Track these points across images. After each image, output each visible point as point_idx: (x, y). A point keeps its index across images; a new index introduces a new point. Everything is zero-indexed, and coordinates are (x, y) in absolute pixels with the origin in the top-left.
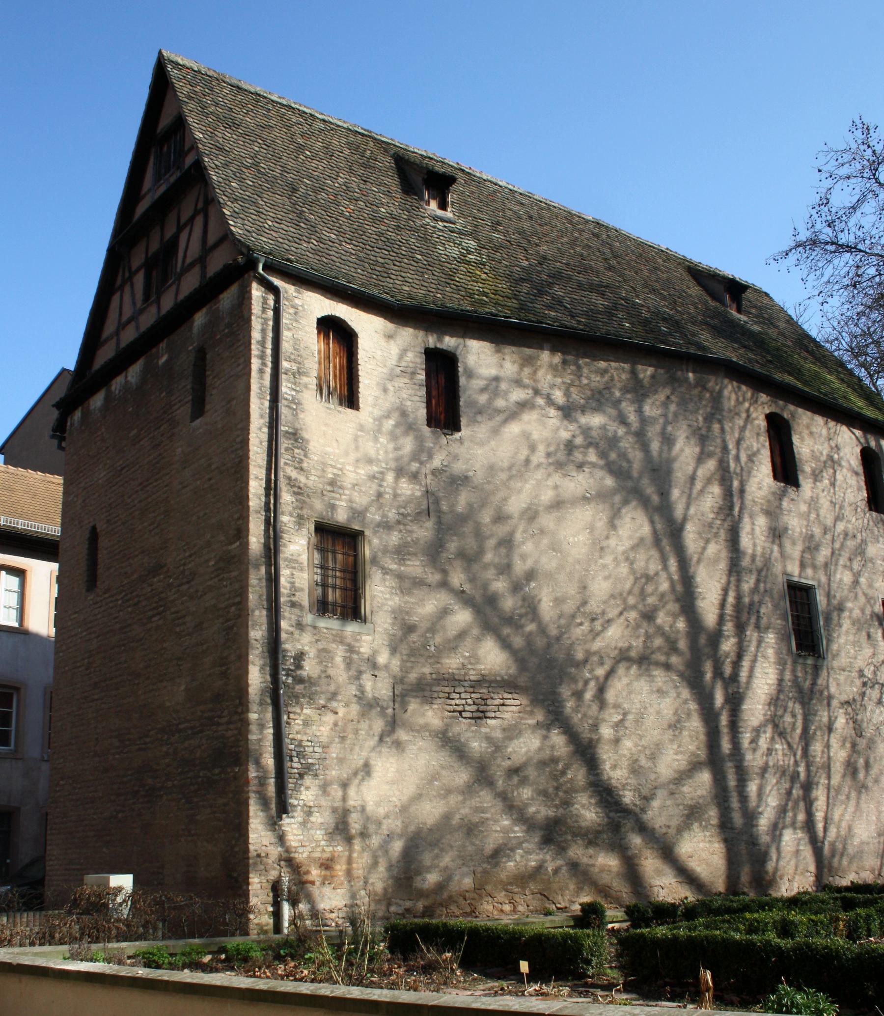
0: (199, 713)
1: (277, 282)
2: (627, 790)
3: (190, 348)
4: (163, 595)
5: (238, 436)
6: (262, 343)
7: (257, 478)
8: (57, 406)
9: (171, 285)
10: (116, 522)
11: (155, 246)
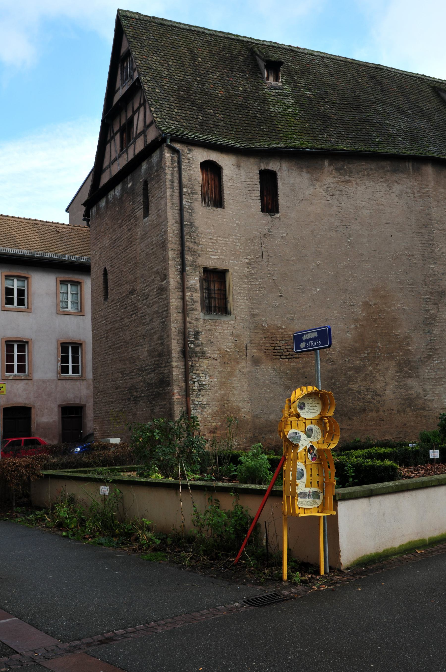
0: (153, 362)
1: (178, 146)
2: (369, 392)
3: (141, 180)
4: (136, 305)
5: (163, 228)
6: (172, 181)
7: (172, 249)
8: (84, 204)
9: (131, 144)
10: (115, 267)
11: (123, 121)
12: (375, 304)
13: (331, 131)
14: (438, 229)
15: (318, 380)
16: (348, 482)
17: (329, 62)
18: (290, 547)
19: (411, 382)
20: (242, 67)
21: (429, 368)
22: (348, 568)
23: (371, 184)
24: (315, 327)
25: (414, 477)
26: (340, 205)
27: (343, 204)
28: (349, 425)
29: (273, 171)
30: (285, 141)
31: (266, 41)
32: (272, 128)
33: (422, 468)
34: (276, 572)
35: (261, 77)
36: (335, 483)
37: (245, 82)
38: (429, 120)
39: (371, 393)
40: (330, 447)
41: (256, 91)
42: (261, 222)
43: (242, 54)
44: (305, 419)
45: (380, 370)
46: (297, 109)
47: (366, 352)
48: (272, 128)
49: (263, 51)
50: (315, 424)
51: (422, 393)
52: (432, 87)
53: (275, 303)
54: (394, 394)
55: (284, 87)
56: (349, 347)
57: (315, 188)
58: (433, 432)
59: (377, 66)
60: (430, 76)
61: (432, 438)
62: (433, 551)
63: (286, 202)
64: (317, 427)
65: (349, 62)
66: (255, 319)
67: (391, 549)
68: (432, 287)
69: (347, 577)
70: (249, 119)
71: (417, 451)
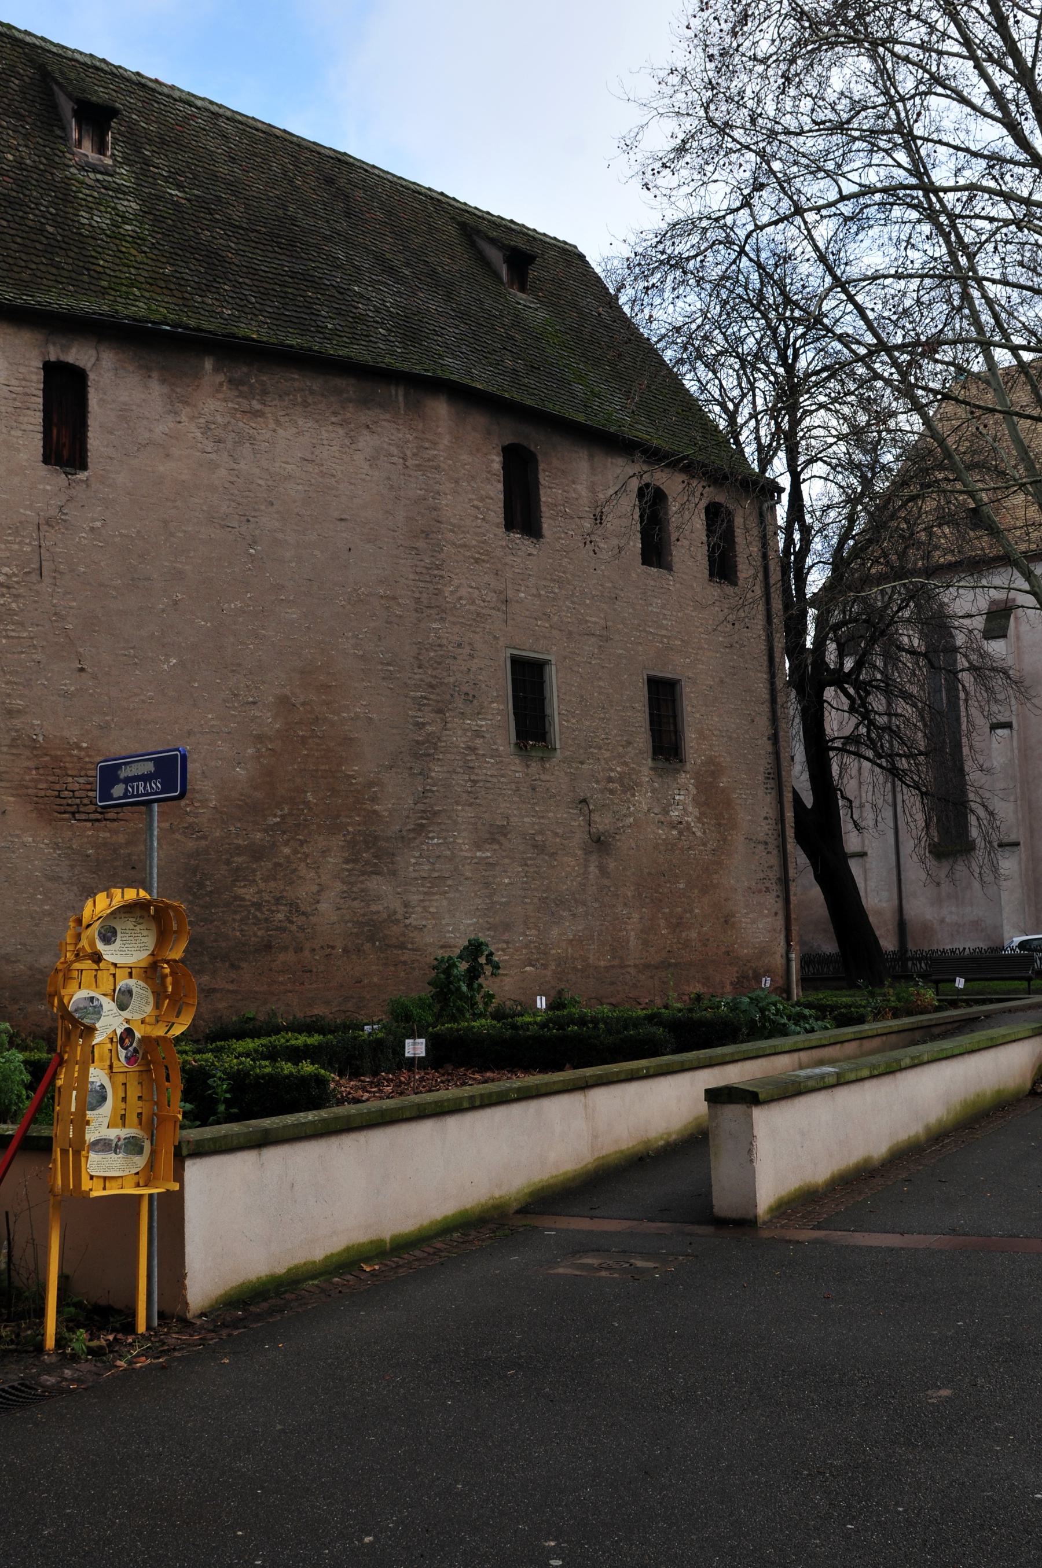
12: (303, 704)
13: (225, 290)
14: (454, 544)
15: (151, 874)
16: (215, 1113)
17: (229, 128)
18: (66, 1271)
19: (376, 884)
20: (16, 104)
21: (417, 854)
22: (203, 1314)
23: (309, 425)
24: (160, 749)
25: (368, 1100)
26: (236, 466)
27: (242, 466)
28: (232, 982)
29: (78, 367)
30: (112, 298)
31: (81, 53)
32: (81, 264)
33: (388, 1080)
34: (29, 1332)
35: (61, 138)
36: (180, 1117)
37: (21, 142)
38: (449, 297)
39: (286, 909)
40: (171, 1032)
41: (48, 168)
42: (41, 487)
43: (19, 74)
44: (115, 965)
45: (307, 856)
46: (147, 227)
47: (279, 813)
48: (81, 264)
49: (72, 76)
50: (139, 978)
51: (400, 910)
52: (458, 224)
53: (65, 685)
54: (338, 912)
55: (118, 170)
56: (239, 800)
57: (178, 419)
58: (420, 999)
59: (339, 156)
60: (458, 198)
61: (416, 1011)
62: (398, 1266)
63: (107, 446)
64: (143, 984)
65: (277, 137)
66: (16, 722)
67: (305, 1264)
68: (434, 673)
69: (200, 1334)
70: (25, 235)
71: (379, 1042)
